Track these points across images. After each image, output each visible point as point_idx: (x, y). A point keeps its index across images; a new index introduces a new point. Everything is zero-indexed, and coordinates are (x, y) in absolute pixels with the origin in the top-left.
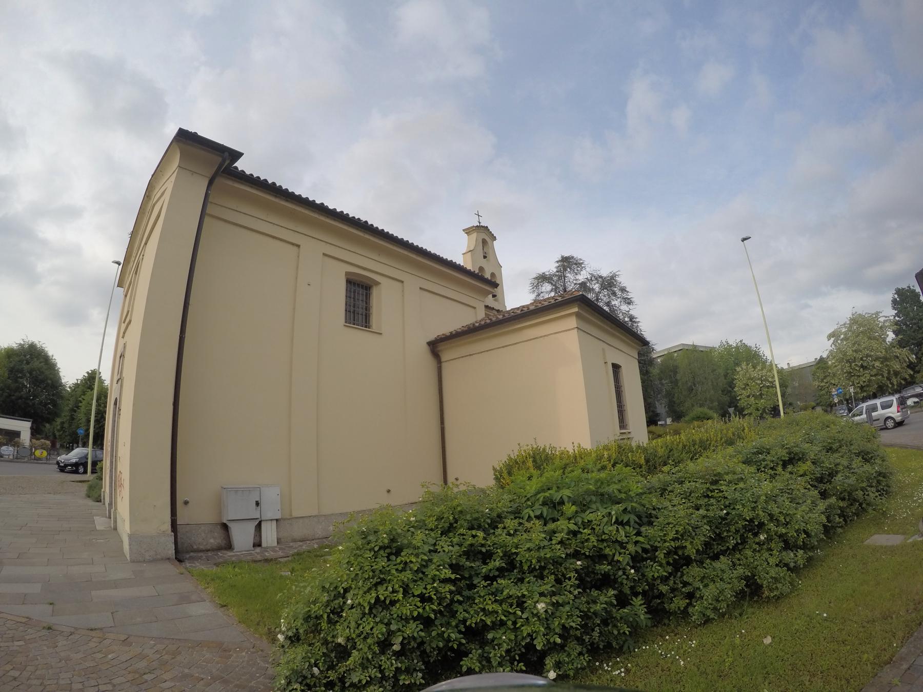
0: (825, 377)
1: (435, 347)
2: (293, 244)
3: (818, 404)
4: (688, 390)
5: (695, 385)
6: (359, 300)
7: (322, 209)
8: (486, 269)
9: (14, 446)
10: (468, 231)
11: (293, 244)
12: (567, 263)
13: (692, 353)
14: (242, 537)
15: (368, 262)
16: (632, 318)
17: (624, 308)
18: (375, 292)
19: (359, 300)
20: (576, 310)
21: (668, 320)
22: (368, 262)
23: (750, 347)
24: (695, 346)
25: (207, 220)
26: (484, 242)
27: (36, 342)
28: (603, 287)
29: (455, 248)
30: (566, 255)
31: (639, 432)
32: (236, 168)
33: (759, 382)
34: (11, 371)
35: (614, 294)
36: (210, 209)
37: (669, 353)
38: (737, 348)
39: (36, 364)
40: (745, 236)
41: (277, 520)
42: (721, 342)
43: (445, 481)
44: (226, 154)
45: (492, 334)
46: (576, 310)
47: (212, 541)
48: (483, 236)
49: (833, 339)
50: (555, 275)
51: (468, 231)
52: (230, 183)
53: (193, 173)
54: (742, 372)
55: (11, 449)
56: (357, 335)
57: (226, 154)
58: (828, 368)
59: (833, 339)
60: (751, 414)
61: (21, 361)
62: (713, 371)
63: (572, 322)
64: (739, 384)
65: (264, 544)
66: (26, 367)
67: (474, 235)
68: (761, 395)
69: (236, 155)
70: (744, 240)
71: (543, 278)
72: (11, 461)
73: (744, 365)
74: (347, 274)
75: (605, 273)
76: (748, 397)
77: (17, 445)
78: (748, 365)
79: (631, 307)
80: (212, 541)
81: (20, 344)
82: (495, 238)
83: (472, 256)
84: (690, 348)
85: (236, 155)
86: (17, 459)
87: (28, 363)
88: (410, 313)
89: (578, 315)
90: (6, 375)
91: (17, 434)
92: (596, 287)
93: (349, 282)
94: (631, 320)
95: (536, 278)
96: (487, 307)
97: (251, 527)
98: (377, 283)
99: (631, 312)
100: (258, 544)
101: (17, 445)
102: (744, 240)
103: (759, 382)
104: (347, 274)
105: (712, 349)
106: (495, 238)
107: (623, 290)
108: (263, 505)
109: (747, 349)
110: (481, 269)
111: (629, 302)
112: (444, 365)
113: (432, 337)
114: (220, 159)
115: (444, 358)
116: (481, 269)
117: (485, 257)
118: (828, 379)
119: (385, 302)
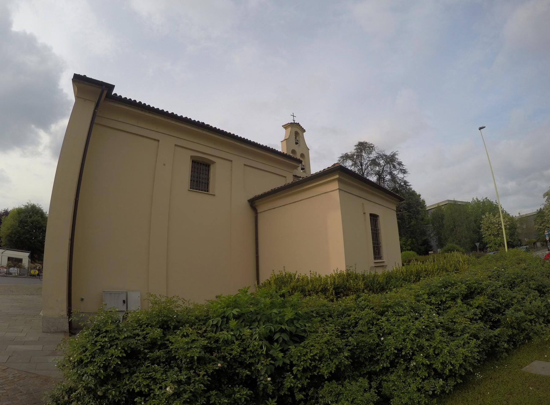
0: (543, 222)
1: (253, 203)
2: (155, 140)
3: (538, 241)
4: (423, 228)
5: (455, 227)
7: (173, 116)
8: (297, 151)
9: (18, 267)
10: (285, 127)
11: (155, 140)
13: (454, 206)
15: (205, 149)
16: (405, 182)
17: (400, 176)
18: (212, 168)
20: (337, 176)
21: (432, 182)
22: (206, 150)
23: (493, 202)
24: (455, 201)
26: (297, 134)
27: (36, 204)
28: (387, 163)
29: (274, 138)
30: (362, 141)
31: (393, 256)
32: (116, 94)
33: (497, 225)
34: (21, 222)
35: (394, 167)
36: (96, 121)
37: (439, 206)
38: (484, 202)
39: (35, 218)
40: (481, 126)
42: (473, 199)
43: (258, 283)
44: (104, 86)
45: (288, 193)
46: (337, 176)
49: (547, 197)
50: (354, 155)
51: (285, 127)
52: (112, 104)
53: (85, 100)
54: (487, 218)
55: (16, 269)
56: (199, 197)
57: (104, 86)
58: (545, 216)
59: (547, 197)
60: (491, 247)
61: (26, 216)
62: (467, 218)
63: (335, 185)
64: (484, 227)
66: (29, 220)
67: (289, 129)
68: (498, 234)
69: (112, 87)
70: (480, 129)
72: (15, 277)
73: (487, 215)
74: (192, 157)
75: (388, 153)
76: (490, 235)
77: (20, 267)
78: (490, 213)
79: (405, 175)
81: (26, 206)
82: (304, 131)
84: (452, 203)
85: (112, 87)
86: (20, 275)
87: (30, 217)
88: (233, 183)
89: (339, 180)
90: (17, 224)
91: (20, 260)
92: (382, 162)
93: (193, 162)
94: (405, 184)
95: (341, 157)
98: (214, 163)
99: (405, 179)
101: (20, 267)
102: (480, 129)
103: (497, 225)
104: (192, 157)
105: (467, 204)
106: (304, 131)
107: (400, 164)
109: (491, 203)
110: (294, 152)
111: (404, 172)
112: (259, 215)
113: (251, 196)
114: (100, 90)
116: (294, 152)
117: (297, 143)
118: (545, 223)
119: (219, 174)
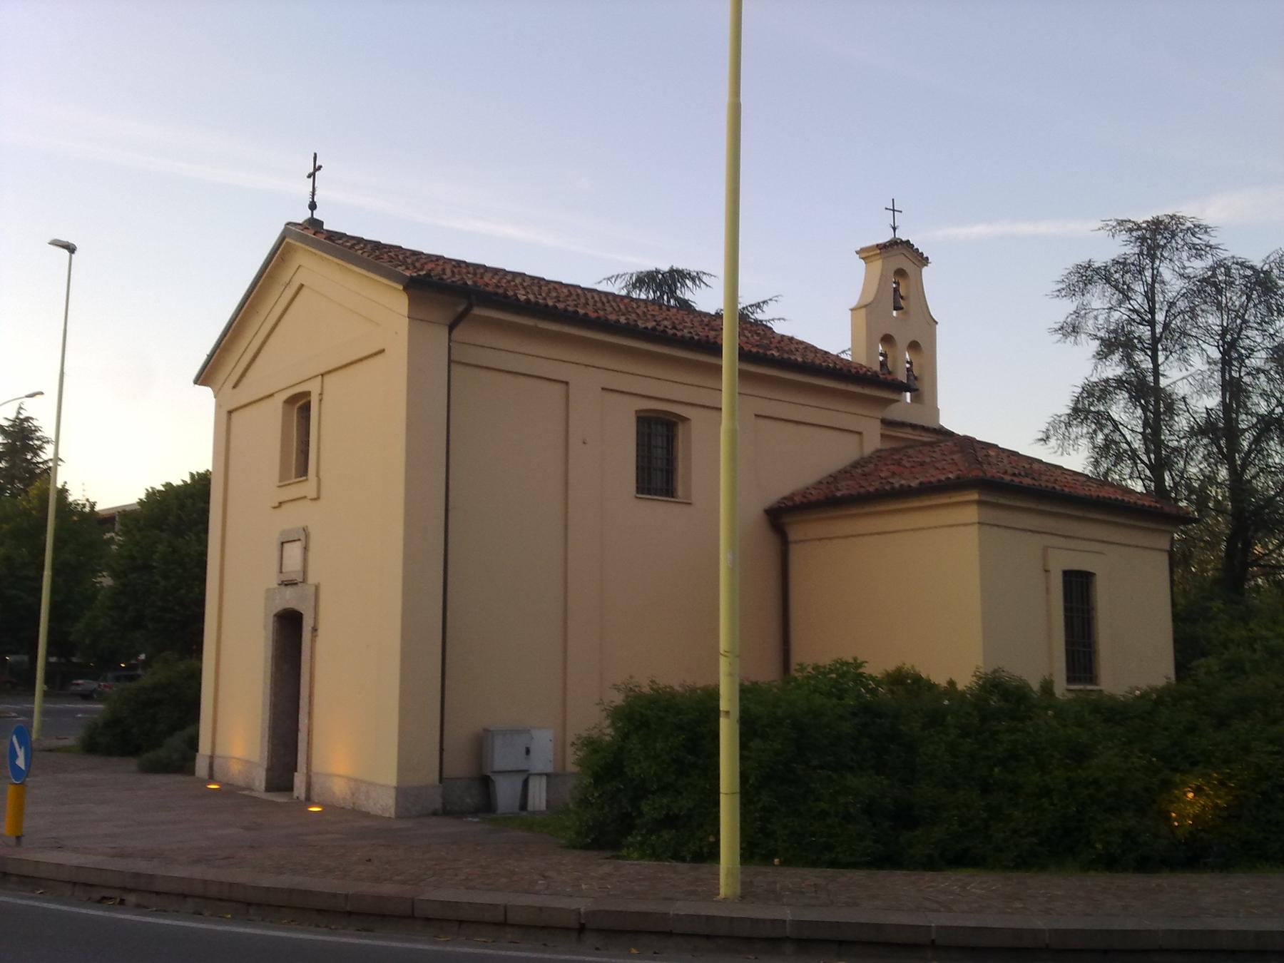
6: (659, 459)
10: (867, 254)
12: (1155, 237)
14: (506, 793)
18: (681, 430)
19: (659, 459)
25: (453, 366)
26: (900, 273)
41: (548, 775)
47: (468, 800)
48: (898, 263)
51: (867, 254)
56: (656, 510)
65: (530, 808)
71: (1086, 276)
80: (468, 800)
83: (868, 315)
96: (886, 423)
97: (519, 780)
98: (685, 420)
100: (523, 806)
108: (532, 754)
115: (792, 536)
